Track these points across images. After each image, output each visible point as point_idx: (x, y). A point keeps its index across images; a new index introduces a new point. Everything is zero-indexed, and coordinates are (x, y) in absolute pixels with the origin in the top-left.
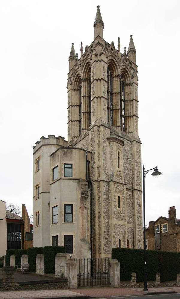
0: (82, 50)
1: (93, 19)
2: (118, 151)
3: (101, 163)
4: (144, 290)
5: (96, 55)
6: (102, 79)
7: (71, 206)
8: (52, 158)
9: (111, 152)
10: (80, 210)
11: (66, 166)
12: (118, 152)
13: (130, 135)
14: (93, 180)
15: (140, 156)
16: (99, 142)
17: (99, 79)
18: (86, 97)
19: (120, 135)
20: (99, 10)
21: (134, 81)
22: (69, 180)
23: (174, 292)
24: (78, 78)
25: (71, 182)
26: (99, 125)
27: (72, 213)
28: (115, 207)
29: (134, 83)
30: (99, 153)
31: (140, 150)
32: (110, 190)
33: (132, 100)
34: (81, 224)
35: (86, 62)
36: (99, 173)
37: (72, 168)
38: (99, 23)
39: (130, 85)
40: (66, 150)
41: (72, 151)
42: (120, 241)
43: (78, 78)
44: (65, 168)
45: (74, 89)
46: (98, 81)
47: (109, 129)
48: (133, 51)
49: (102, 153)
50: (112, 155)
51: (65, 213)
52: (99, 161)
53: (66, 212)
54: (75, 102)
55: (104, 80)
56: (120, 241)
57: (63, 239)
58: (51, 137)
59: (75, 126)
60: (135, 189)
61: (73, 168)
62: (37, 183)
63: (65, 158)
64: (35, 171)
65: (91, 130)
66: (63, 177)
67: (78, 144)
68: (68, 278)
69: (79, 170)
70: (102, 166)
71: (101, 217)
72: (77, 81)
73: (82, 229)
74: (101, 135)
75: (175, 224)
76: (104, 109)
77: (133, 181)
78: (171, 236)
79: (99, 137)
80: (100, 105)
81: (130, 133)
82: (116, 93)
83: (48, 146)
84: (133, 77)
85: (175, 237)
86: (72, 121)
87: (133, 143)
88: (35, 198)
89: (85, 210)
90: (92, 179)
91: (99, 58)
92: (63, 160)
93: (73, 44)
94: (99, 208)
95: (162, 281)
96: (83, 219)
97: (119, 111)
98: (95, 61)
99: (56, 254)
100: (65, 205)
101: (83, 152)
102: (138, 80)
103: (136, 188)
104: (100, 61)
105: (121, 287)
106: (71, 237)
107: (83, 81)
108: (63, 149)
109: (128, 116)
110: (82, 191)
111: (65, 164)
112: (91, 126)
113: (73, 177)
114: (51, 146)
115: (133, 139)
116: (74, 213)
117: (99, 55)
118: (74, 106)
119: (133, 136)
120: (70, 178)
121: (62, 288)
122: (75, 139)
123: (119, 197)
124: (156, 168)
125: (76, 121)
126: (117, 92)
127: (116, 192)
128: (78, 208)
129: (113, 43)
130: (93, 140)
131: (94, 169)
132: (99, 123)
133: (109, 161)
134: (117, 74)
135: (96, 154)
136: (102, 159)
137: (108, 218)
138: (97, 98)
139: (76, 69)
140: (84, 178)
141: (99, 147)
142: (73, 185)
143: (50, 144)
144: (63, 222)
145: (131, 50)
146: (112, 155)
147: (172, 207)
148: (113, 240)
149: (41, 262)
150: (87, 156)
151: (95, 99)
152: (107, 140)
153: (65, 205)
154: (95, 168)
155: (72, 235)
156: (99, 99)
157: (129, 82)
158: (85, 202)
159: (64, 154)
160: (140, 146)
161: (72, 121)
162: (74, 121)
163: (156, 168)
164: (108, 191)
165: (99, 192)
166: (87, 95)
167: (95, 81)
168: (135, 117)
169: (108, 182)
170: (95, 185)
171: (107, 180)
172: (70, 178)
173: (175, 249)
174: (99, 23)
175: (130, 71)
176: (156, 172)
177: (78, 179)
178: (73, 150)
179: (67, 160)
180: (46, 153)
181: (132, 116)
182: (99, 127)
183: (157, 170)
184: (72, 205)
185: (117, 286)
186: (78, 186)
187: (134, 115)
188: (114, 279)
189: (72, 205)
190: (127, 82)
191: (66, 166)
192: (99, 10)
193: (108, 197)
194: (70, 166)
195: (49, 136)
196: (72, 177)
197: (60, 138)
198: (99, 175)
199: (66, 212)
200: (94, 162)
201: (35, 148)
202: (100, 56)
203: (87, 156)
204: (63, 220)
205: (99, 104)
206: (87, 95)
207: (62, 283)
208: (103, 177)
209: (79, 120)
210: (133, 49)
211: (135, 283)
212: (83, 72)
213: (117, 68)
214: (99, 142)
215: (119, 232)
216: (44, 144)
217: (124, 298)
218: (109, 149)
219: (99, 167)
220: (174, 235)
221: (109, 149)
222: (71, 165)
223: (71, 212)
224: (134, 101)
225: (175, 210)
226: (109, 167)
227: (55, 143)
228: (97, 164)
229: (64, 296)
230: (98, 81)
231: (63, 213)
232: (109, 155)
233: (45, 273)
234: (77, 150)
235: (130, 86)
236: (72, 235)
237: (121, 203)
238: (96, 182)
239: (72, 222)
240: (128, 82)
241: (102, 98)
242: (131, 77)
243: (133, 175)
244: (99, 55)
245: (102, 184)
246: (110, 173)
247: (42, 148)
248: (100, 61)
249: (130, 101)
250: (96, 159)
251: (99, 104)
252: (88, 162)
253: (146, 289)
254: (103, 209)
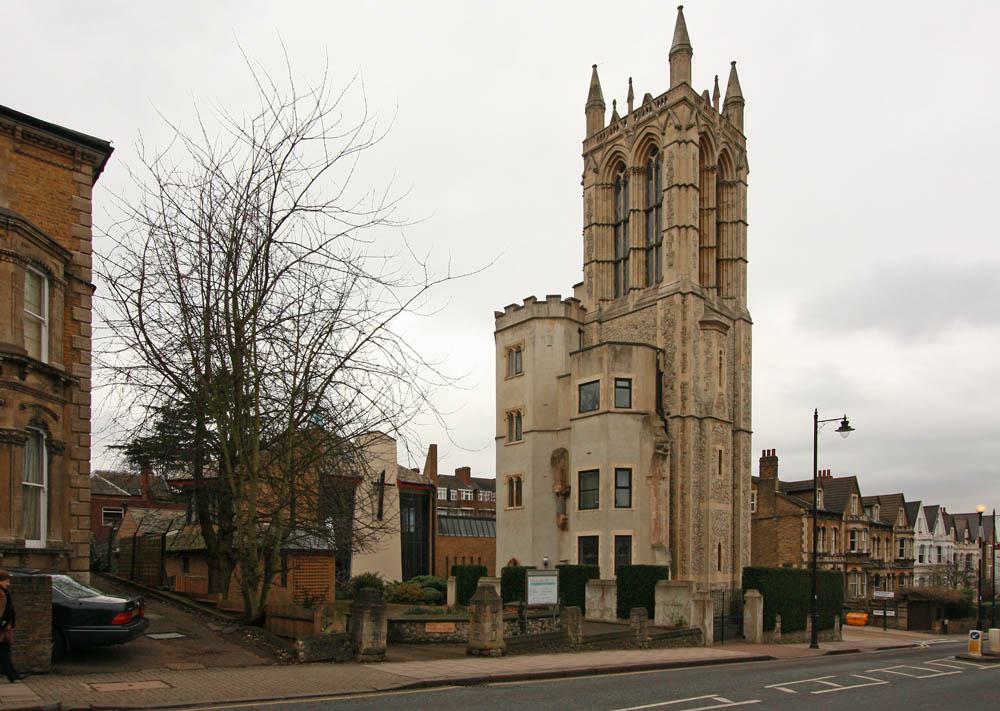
0: (630, 99)
1: (667, 42)
2: (721, 349)
3: (688, 377)
4: (811, 647)
5: (678, 128)
6: (692, 185)
7: (627, 473)
8: (579, 360)
9: (707, 352)
10: (650, 482)
11: (620, 383)
12: (721, 352)
13: (729, 304)
14: (668, 414)
15: (749, 353)
16: (684, 329)
17: (684, 185)
18: (638, 211)
19: (716, 308)
20: (681, 16)
21: (742, 178)
22: (624, 416)
23: (768, 658)
24: (615, 160)
25: (629, 420)
26: (684, 292)
27: (629, 488)
28: (714, 474)
29: (741, 181)
30: (684, 355)
31: (750, 339)
32: (704, 436)
33: (737, 223)
34: (654, 513)
35: (644, 133)
36: (684, 399)
37: (630, 388)
38: (682, 52)
39: (732, 185)
40: (618, 347)
41: (631, 350)
42: (720, 546)
43: (615, 160)
44: (616, 387)
45: (602, 184)
46: (683, 188)
47: (702, 301)
48: (736, 102)
49: (690, 357)
50: (709, 360)
51: (616, 487)
52: (683, 372)
53: (619, 485)
54: (605, 215)
55: (695, 187)
56: (720, 546)
57: (613, 543)
58: (553, 299)
59: (605, 275)
60: (740, 430)
61: (634, 387)
62: (511, 406)
63: (617, 366)
64: (504, 374)
65: (665, 301)
66: (613, 409)
67: (617, 320)
68: (701, 627)
69: (643, 395)
70: (691, 385)
71: (687, 497)
72: (611, 167)
73: (656, 524)
74: (690, 315)
75: (776, 494)
76: (694, 255)
77: (737, 409)
78: (766, 521)
79: (684, 320)
80: (686, 244)
81: (731, 299)
82: (708, 210)
83: (547, 321)
84: (739, 169)
85: (776, 526)
86: (598, 262)
87: (737, 323)
88: (504, 441)
89: (662, 482)
90: (666, 411)
91: (684, 136)
92: (613, 370)
93: (595, 66)
94: (683, 477)
95: (783, 631)
96: (659, 501)
97: (715, 251)
98: (676, 141)
99: (655, 583)
100: (617, 470)
101: (651, 351)
102: (748, 173)
103: (742, 427)
104: (687, 143)
105: (765, 642)
106: (629, 538)
107: (634, 173)
108: (612, 346)
109: (727, 260)
110: (656, 442)
111: (617, 379)
112: (663, 290)
113: (634, 409)
114: (553, 321)
115: (737, 315)
116: (634, 488)
117: (684, 127)
118: (603, 225)
119: (737, 307)
120: (625, 410)
121: (694, 645)
122: (606, 307)
123: (720, 451)
124: (845, 418)
125: (608, 262)
126: (711, 206)
127: (716, 441)
128: (645, 478)
129: (706, 92)
130: (670, 323)
131: (672, 388)
132: (684, 286)
133: (702, 372)
134: (711, 164)
135: (678, 357)
136: (690, 366)
137: (701, 498)
138: (680, 228)
139: (611, 137)
140: (652, 409)
141: (683, 342)
142: (634, 424)
143: (551, 315)
144: (613, 508)
145: (735, 99)
146: (709, 360)
147: (769, 451)
148: (710, 546)
149: (605, 597)
150: (658, 361)
151: (675, 232)
152: (699, 326)
153: (617, 470)
154: (675, 388)
155: (631, 536)
156: (683, 229)
157: (730, 179)
158: (662, 464)
159: (615, 357)
160: (750, 329)
161: (598, 262)
162: (603, 262)
163: (845, 418)
164: (702, 437)
165: (684, 442)
166: (641, 208)
167: (677, 188)
168: (741, 263)
169: (701, 420)
170: (675, 425)
171: (698, 415)
172: (625, 410)
173: (774, 554)
174: (682, 52)
175: (733, 153)
176: (845, 426)
177: (643, 414)
178: (634, 348)
179: (620, 371)
180: (542, 338)
181: (736, 260)
182: (684, 295)
183: (848, 422)
184: (630, 470)
185: (759, 640)
186: (644, 428)
187: (741, 259)
188: (753, 627)
189: (630, 470)
190: (725, 178)
191: (620, 383)
192: (681, 16)
193: (701, 451)
194: (626, 384)
195: (548, 297)
196: (630, 407)
197: (572, 302)
198: (684, 404)
199: (619, 485)
200: (674, 374)
201: (501, 319)
202: (687, 129)
203: (658, 361)
204: (613, 503)
205: (683, 242)
206: (641, 208)
207: (680, 635)
208: (692, 410)
209: (613, 259)
210: (686, 47)
211: (780, 634)
212: (634, 151)
213: (712, 149)
214: (684, 329)
215: (719, 526)
216: (536, 315)
217: (310, 706)
218: (702, 346)
219: (684, 386)
220: (771, 521)
221: (702, 346)
222: (629, 380)
223: (627, 485)
224: (741, 224)
225: (775, 459)
226: (702, 385)
227: (563, 315)
228: (680, 378)
229: (447, 676)
230: (683, 188)
231: (613, 487)
232: (702, 358)
233: (618, 617)
234: (640, 348)
235: (732, 187)
236: (631, 536)
237: (723, 465)
238: (676, 420)
239: (630, 506)
240: (728, 178)
241: (690, 230)
242: (734, 167)
243: (735, 396)
244: (684, 127)
245: (691, 424)
246: (704, 397)
247: (532, 323)
248: (687, 143)
249: (731, 223)
250: (677, 365)
251: (683, 242)
252: (659, 375)
253: (814, 645)
254: (693, 478)
